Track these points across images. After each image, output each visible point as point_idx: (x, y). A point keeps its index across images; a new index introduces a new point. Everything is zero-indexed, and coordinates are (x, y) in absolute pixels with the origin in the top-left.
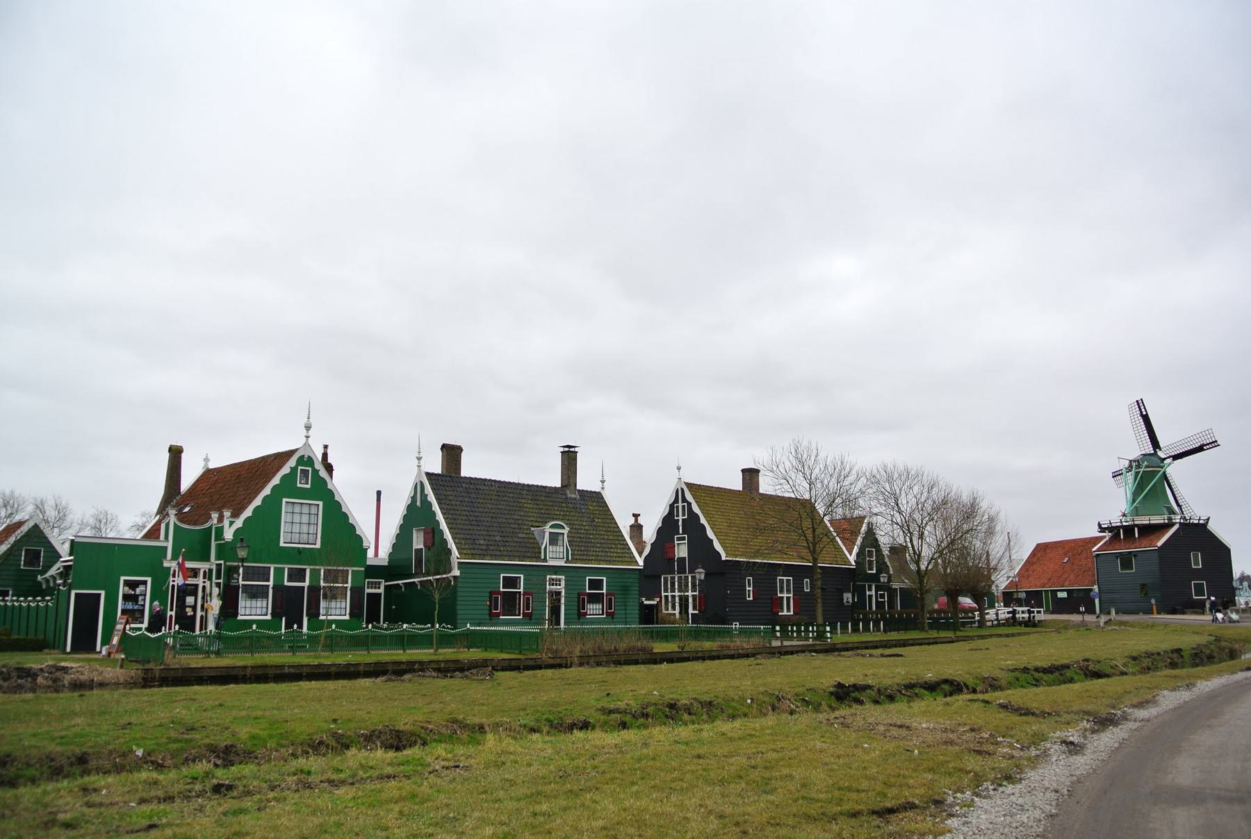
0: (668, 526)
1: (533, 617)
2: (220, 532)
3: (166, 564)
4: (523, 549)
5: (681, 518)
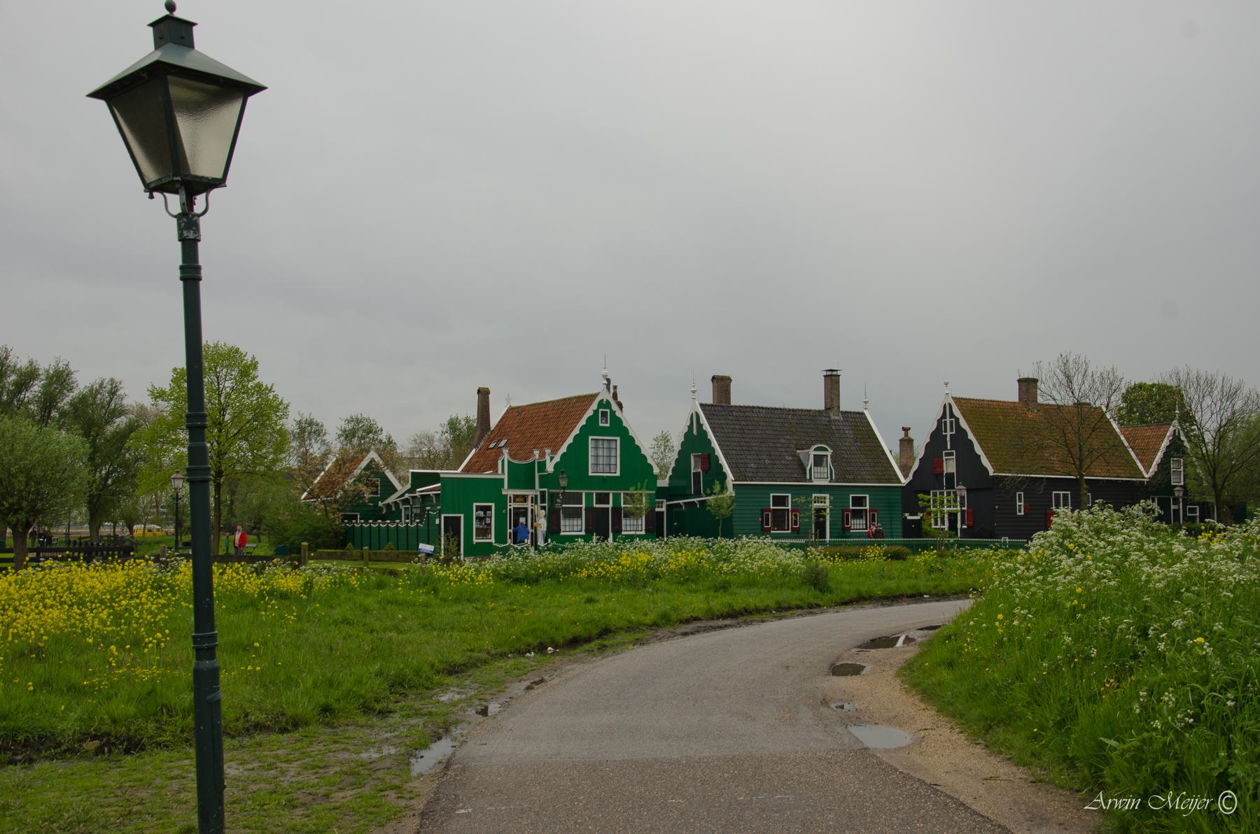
0: (937, 439)
1: (801, 531)
2: (542, 466)
3: (503, 493)
4: (790, 471)
5: (948, 433)
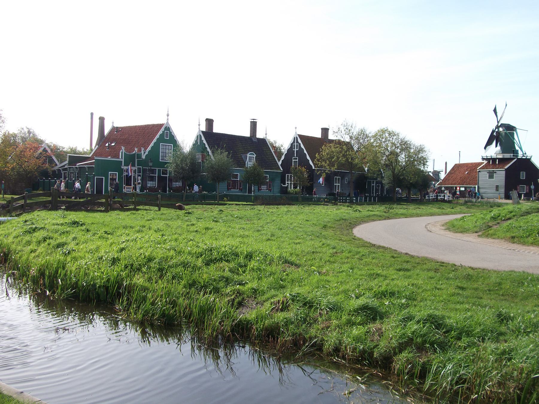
3: (122, 168)
5: (295, 150)
